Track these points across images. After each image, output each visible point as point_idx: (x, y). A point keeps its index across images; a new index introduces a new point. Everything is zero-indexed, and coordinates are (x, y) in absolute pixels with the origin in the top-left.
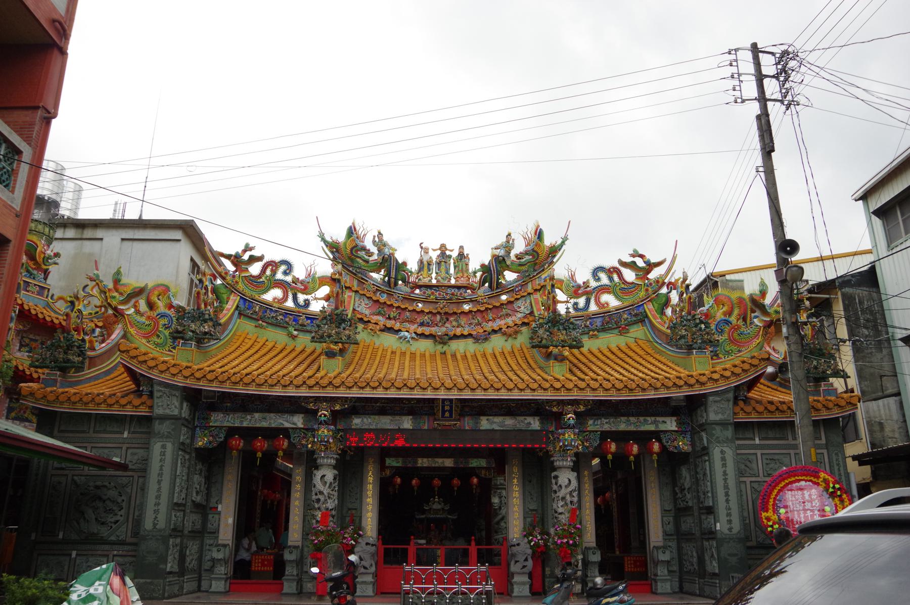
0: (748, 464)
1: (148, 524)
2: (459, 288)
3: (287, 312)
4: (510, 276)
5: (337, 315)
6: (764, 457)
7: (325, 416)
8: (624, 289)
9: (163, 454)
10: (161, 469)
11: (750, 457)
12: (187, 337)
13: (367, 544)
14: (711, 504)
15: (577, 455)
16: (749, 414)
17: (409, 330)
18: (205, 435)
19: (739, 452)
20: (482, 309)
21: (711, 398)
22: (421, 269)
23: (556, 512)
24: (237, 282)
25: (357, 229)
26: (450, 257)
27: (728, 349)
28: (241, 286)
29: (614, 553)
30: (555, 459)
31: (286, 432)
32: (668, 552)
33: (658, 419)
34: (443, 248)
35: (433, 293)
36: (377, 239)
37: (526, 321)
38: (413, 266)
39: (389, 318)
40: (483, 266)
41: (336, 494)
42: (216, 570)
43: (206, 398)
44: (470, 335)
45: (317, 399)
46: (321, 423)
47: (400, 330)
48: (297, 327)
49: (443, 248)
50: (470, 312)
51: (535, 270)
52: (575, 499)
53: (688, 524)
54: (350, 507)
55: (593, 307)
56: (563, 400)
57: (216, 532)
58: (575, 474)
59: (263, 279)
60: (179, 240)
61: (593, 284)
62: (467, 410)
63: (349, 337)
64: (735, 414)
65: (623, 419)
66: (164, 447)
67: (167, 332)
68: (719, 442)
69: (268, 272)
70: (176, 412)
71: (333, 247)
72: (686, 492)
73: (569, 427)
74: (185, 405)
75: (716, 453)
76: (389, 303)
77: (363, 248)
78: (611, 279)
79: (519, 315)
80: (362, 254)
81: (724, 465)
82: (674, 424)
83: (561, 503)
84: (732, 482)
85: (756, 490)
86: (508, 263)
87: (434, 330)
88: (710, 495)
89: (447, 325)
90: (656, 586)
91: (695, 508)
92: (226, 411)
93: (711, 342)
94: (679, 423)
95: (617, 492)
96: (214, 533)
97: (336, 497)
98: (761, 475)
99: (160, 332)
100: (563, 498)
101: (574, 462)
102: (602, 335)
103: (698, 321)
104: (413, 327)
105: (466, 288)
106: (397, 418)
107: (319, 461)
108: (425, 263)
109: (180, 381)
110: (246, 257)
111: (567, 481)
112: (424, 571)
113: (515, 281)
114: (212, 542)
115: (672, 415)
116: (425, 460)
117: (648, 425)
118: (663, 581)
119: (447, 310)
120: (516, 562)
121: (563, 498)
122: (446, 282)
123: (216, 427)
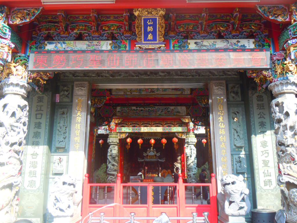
13: (64, 183)
116: (145, 128)
120: (231, 203)
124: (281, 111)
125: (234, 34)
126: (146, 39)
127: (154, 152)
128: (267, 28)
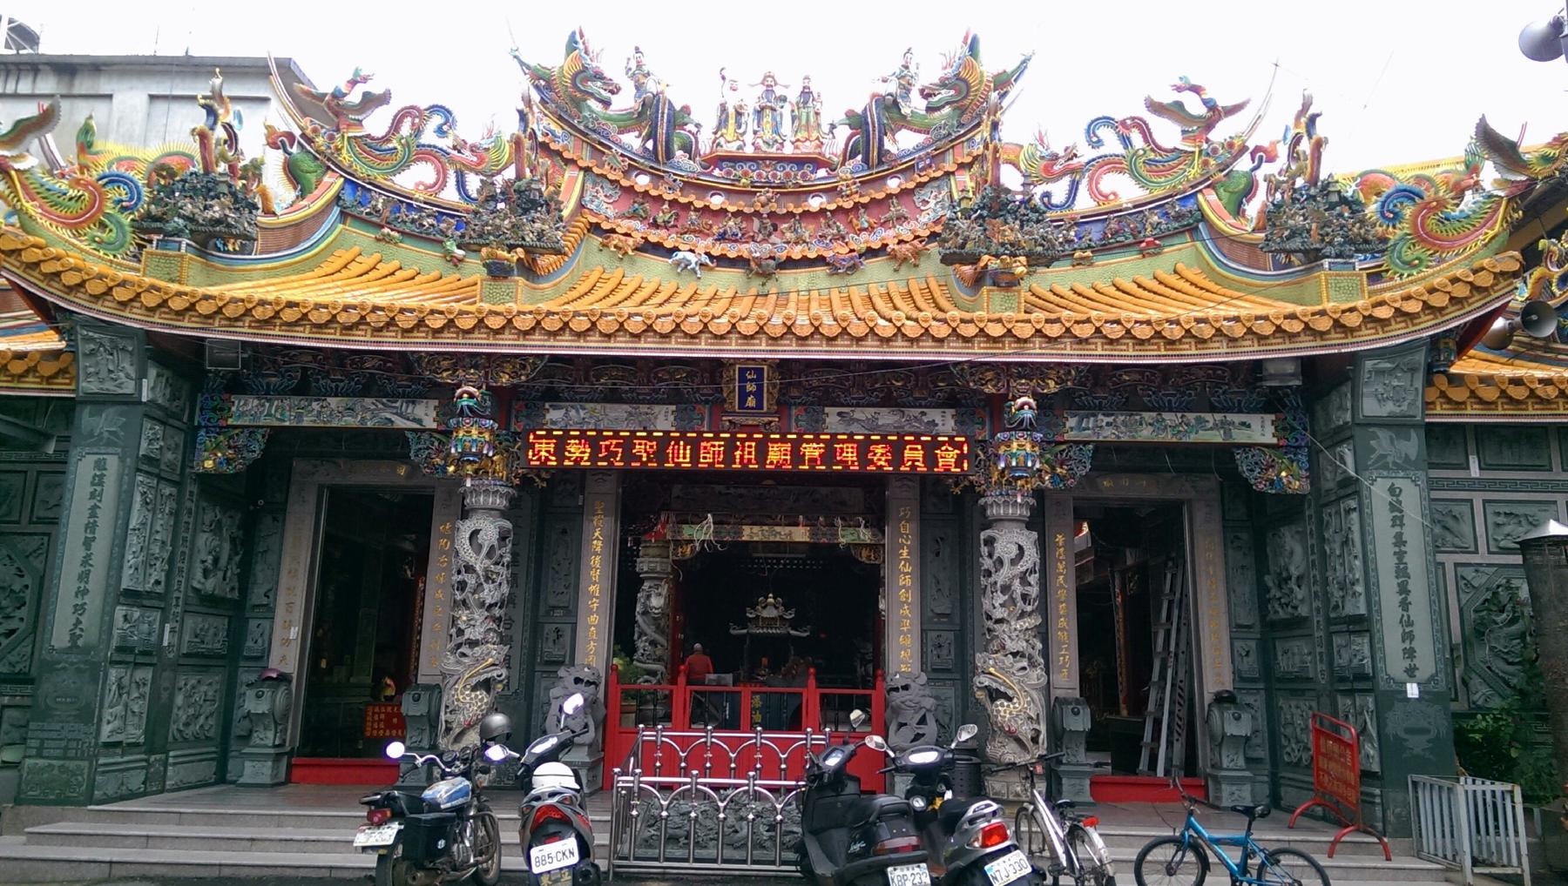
0: (1450, 523)
1: (60, 637)
2: (800, 162)
3: (444, 212)
4: (905, 142)
5: (518, 191)
6: (1490, 509)
7: (471, 396)
8: (1160, 161)
9: (98, 481)
10: (93, 515)
11: (1456, 509)
14: (1363, 610)
15: (1039, 494)
16: (1459, 405)
17: (694, 249)
19: (1435, 494)
20: (848, 205)
21: (1369, 364)
22: (722, 123)
23: (989, 617)
24: (338, 150)
27: (1409, 255)
28: (346, 157)
29: (1118, 713)
30: (990, 500)
32: (1246, 717)
33: (1230, 417)
34: (769, 83)
35: (746, 174)
39: (655, 225)
40: (850, 115)
44: (821, 260)
46: (462, 413)
47: (676, 249)
49: (769, 83)
50: (823, 211)
51: (961, 125)
52: (1034, 591)
53: (1296, 656)
54: (552, 602)
55: (1084, 203)
56: (1008, 364)
58: (1035, 535)
59: (394, 144)
60: (265, 100)
61: (1086, 153)
62: (794, 393)
63: (540, 235)
64: (1427, 405)
65: (1148, 416)
66: (100, 465)
67: (126, 220)
68: (1385, 467)
69: (406, 129)
70: (129, 388)
71: (543, 80)
72: (1293, 584)
73: (1020, 426)
75: (1378, 491)
76: (654, 193)
78: (1126, 141)
79: (924, 219)
80: (595, 86)
81: (1398, 521)
82: (1270, 429)
84: (1416, 561)
85: (1468, 584)
86: (905, 110)
87: (744, 249)
88: (1359, 588)
89: (773, 238)
90: (1218, 790)
92: (267, 393)
93: (1366, 241)
94: (1280, 429)
98: (1482, 548)
99: (107, 215)
100: (1006, 589)
101: (1032, 508)
102: (1100, 261)
103: (1335, 198)
104: (703, 244)
106: (644, 408)
108: (731, 111)
109: (134, 320)
110: (355, 97)
111: (1014, 551)
112: (683, 742)
115: (1266, 409)
116: (756, 529)
118: (1233, 781)
119: (774, 207)
120: (902, 725)
121: (1006, 589)
122: (773, 151)
125: (917, 395)
128: (584, 781)
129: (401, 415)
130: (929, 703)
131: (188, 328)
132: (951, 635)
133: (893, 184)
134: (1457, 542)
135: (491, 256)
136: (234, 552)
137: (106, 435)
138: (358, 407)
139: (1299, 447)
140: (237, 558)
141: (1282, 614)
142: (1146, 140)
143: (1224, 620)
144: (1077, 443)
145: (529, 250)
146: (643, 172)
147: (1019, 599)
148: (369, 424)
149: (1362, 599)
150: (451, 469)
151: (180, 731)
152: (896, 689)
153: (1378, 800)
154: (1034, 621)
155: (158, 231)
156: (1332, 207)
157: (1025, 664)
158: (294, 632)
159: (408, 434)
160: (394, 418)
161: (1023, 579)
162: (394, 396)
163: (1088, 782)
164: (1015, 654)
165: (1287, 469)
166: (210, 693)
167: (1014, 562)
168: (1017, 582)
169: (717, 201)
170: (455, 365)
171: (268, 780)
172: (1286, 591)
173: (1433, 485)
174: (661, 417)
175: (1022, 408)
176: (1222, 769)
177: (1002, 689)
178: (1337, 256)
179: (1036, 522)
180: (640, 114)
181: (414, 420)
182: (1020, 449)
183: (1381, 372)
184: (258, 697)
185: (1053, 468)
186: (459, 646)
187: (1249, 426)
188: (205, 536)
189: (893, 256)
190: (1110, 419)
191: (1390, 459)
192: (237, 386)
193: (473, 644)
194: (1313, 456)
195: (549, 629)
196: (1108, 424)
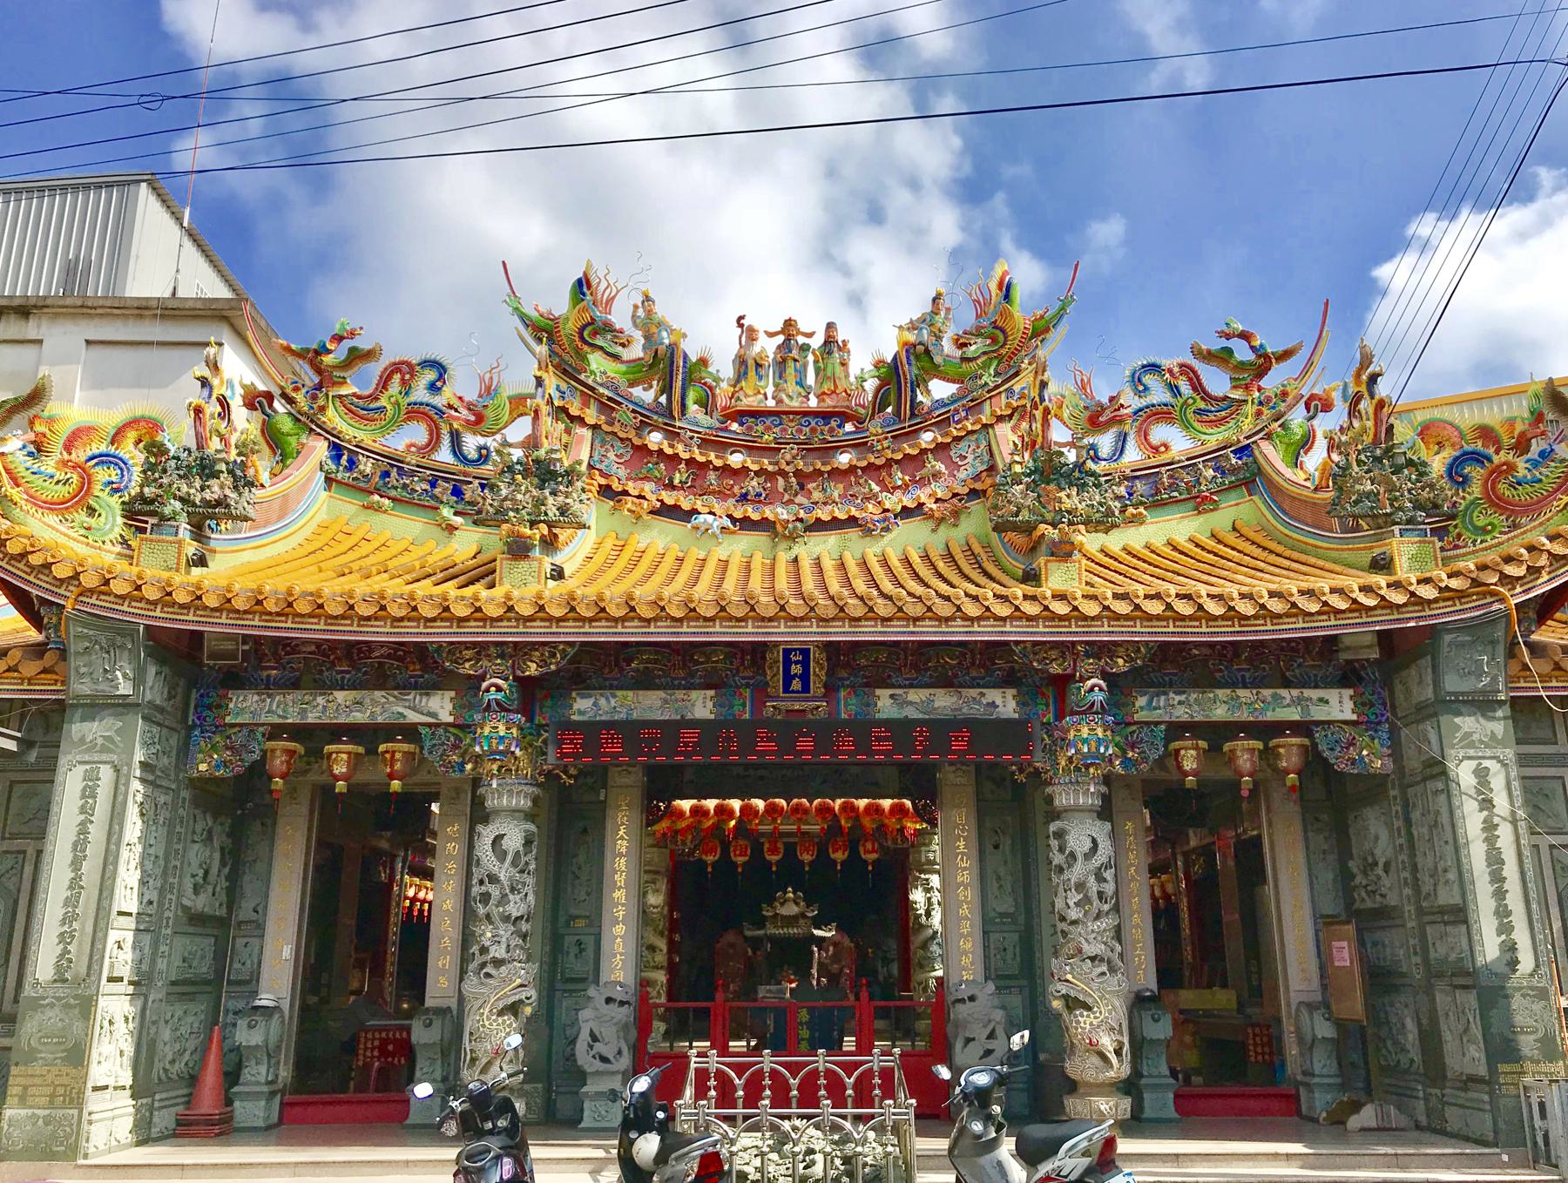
2: (826, 416)
7: (499, 689)
12: (167, 510)
13: (609, 1000)
17: (713, 514)
18: (214, 747)
20: (879, 462)
21: (1448, 638)
23: (1063, 919)
25: (594, 284)
26: (805, 348)
27: (1481, 522)
28: (334, 418)
31: (410, 732)
33: (1307, 693)
36: (641, 312)
37: (978, 486)
38: (723, 367)
41: (530, 880)
42: (246, 1075)
43: (212, 656)
44: (852, 521)
45: (481, 649)
47: (695, 512)
48: (460, 507)
50: (852, 469)
52: (1109, 888)
57: (251, 983)
61: (1131, 401)
65: (1222, 693)
72: (1380, 871)
74: (152, 670)
77: (608, 328)
78: (1174, 390)
79: (962, 475)
82: (1349, 705)
83: (1074, 897)
86: (938, 359)
91: (1409, 908)
92: (268, 686)
94: (1358, 705)
95: (1187, 874)
96: (248, 982)
97: (530, 890)
100: (1080, 886)
103: (1402, 460)
105: (844, 417)
106: (680, 694)
107: (488, 804)
108: (751, 363)
111: (1088, 845)
112: (794, 1069)
113: (954, 399)
114: (240, 1005)
117: (1285, 706)
120: (968, 1040)
121: (1080, 886)
123: (241, 725)
124: (1061, 850)
125: (974, 674)
126: (786, 690)
127: (797, 904)
129: (414, 709)
130: (999, 1015)
131: (190, 621)
132: (1016, 937)
133: (927, 438)
134: (1550, 822)
135: (511, 534)
136: (223, 863)
137: (100, 741)
138: (367, 701)
139: (1379, 723)
140: (227, 870)
141: (1369, 904)
142: (1194, 389)
143: (1307, 912)
144: (1148, 723)
145: (550, 525)
146: (656, 428)
147: (1095, 897)
148: (380, 720)
149: (1456, 888)
150: (469, 767)
151: (166, 1070)
152: (962, 1001)
153: (1488, 1107)
154: (1106, 923)
155: (153, 514)
156: (1397, 470)
157: (1104, 968)
158: (287, 952)
159: (423, 730)
160: (407, 712)
161: (1100, 879)
162: (405, 687)
163: (1171, 1096)
164: (1093, 959)
165: (1367, 746)
166: (196, 1025)
167: (1088, 856)
168: (1092, 879)
169: (736, 460)
170: (478, 653)
171: (261, 1123)
172: (1373, 877)
173: (1523, 760)
174: (699, 704)
175: (1092, 689)
176: (1313, 1075)
177: (1081, 998)
178: (1409, 522)
179: (1105, 812)
180: (651, 366)
181: (429, 714)
182: (1088, 734)
183: (1462, 645)
184: (250, 1027)
185: (1124, 752)
186: (483, 965)
187: (1327, 702)
188: (196, 846)
189: (930, 516)
190: (1183, 698)
191: (1475, 737)
192: (235, 680)
193: (498, 963)
194: (1394, 734)
195: (569, 941)
196: (1180, 703)
